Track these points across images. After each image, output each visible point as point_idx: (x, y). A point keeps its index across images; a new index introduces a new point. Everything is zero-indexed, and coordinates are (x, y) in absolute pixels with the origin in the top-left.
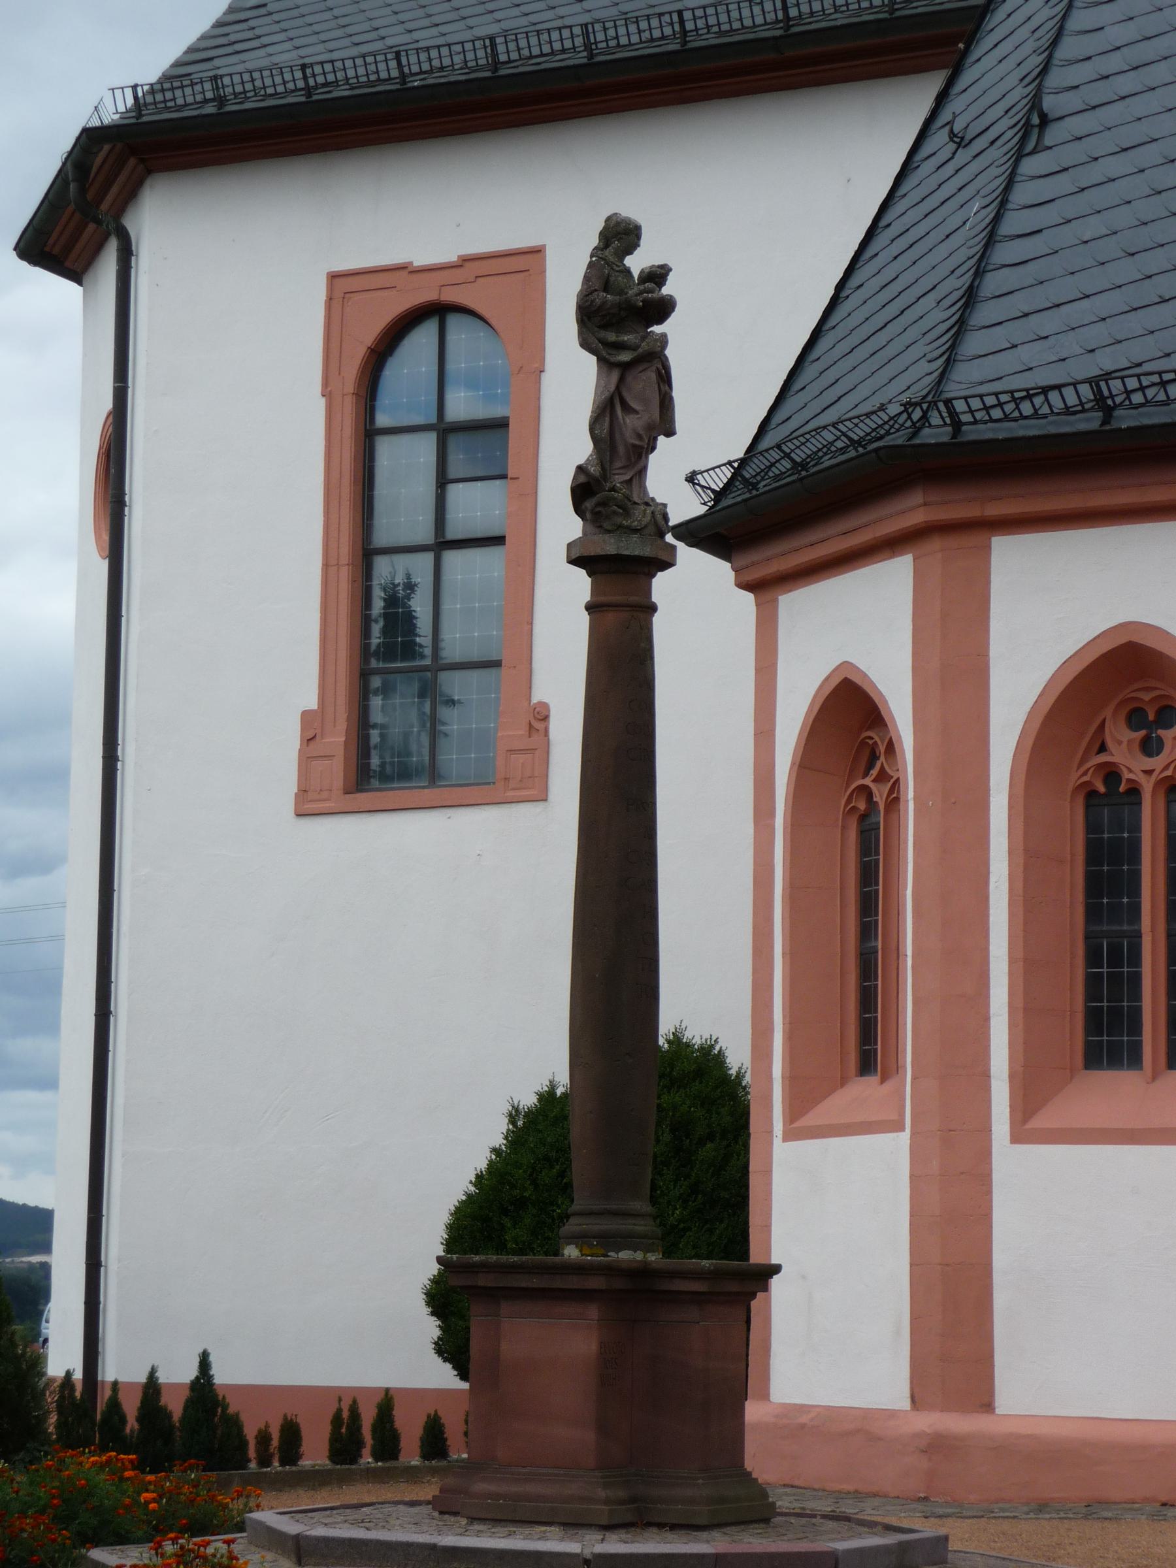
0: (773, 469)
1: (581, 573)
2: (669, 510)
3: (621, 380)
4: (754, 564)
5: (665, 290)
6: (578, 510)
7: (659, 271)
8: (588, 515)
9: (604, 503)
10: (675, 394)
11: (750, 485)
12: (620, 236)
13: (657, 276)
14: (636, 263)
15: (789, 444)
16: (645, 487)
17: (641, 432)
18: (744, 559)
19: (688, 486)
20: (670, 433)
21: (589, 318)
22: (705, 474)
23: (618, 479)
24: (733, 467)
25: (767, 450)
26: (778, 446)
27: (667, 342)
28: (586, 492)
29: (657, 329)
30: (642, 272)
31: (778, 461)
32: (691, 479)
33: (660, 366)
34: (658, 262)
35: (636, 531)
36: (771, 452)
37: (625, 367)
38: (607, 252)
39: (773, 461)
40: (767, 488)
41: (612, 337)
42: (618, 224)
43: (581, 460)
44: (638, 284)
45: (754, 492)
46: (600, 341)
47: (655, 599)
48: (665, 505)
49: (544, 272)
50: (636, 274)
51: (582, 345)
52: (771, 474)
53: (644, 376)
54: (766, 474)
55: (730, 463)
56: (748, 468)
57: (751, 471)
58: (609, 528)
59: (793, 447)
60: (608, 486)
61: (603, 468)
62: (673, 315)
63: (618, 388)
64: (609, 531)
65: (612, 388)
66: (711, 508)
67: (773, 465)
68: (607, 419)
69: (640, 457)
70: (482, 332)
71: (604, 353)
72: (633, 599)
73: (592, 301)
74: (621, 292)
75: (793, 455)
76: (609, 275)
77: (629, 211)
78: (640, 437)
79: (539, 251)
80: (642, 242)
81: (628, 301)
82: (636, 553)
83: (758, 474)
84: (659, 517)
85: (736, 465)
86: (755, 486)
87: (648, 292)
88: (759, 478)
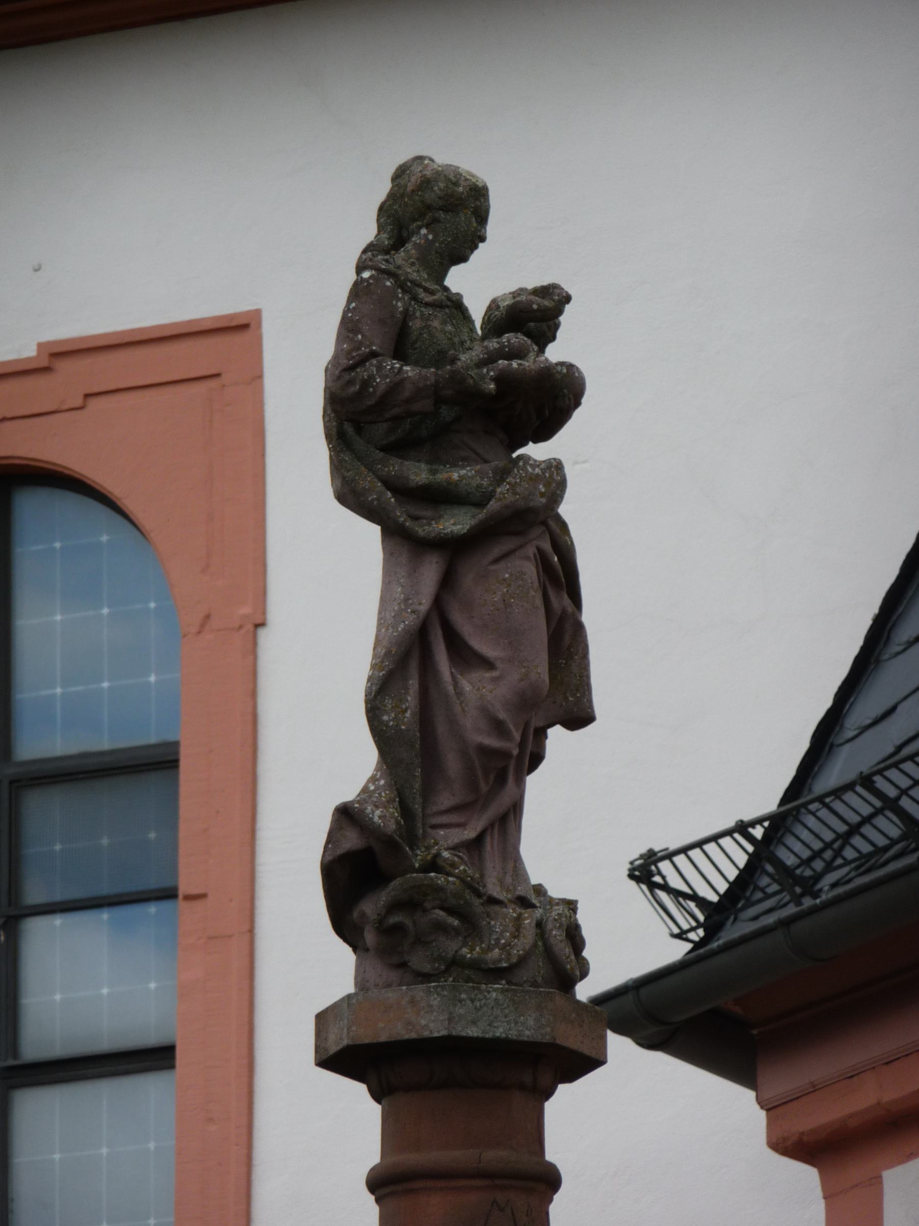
0: (857, 841)
1: (354, 1093)
2: (582, 917)
3: (447, 582)
4: (814, 1089)
5: (554, 353)
6: (344, 923)
7: (537, 303)
8: (370, 937)
9: (410, 903)
10: (589, 617)
11: (797, 882)
12: (434, 215)
13: (534, 315)
14: (478, 284)
15: (893, 774)
16: (517, 860)
17: (502, 715)
18: (786, 1079)
19: (636, 893)
20: (579, 717)
21: (359, 430)
22: (680, 860)
23: (446, 840)
24: (750, 838)
25: (837, 792)
26: (866, 781)
27: (562, 485)
28: (362, 873)
29: (536, 451)
30: (494, 305)
31: (867, 820)
32: (644, 872)
33: (547, 546)
34: (533, 279)
35: (496, 973)
36: (849, 797)
37: (455, 550)
38: (399, 257)
39: (854, 819)
40: (840, 890)
41: (418, 473)
42: (426, 183)
43: (349, 793)
44: (484, 338)
45: (808, 902)
46: (389, 484)
47: (552, 1154)
48: (572, 905)
49: (258, 378)
50: (477, 312)
51: (342, 498)
52: (849, 853)
53: (505, 571)
54: (838, 853)
55: (742, 828)
56: (790, 840)
57: (797, 847)
58: (427, 968)
59: (905, 783)
60: (419, 857)
61: (405, 811)
62: (577, 414)
63: (438, 603)
64: (424, 977)
65: (424, 603)
66: (697, 945)
67: (854, 830)
68: (414, 684)
69: (501, 780)
70: (104, 532)
71: (401, 516)
72: (493, 1157)
73: (365, 384)
74: (441, 358)
75: (905, 803)
76: (407, 315)
77: (456, 149)
78: (498, 727)
79: (244, 327)
80: (491, 229)
81: (457, 379)
82: (499, 1032)
83: (816, 855)
84: (557, 935)
85: (758, 832)
86: (810, 886)
87: (510, 357)
88: (818, 865)
